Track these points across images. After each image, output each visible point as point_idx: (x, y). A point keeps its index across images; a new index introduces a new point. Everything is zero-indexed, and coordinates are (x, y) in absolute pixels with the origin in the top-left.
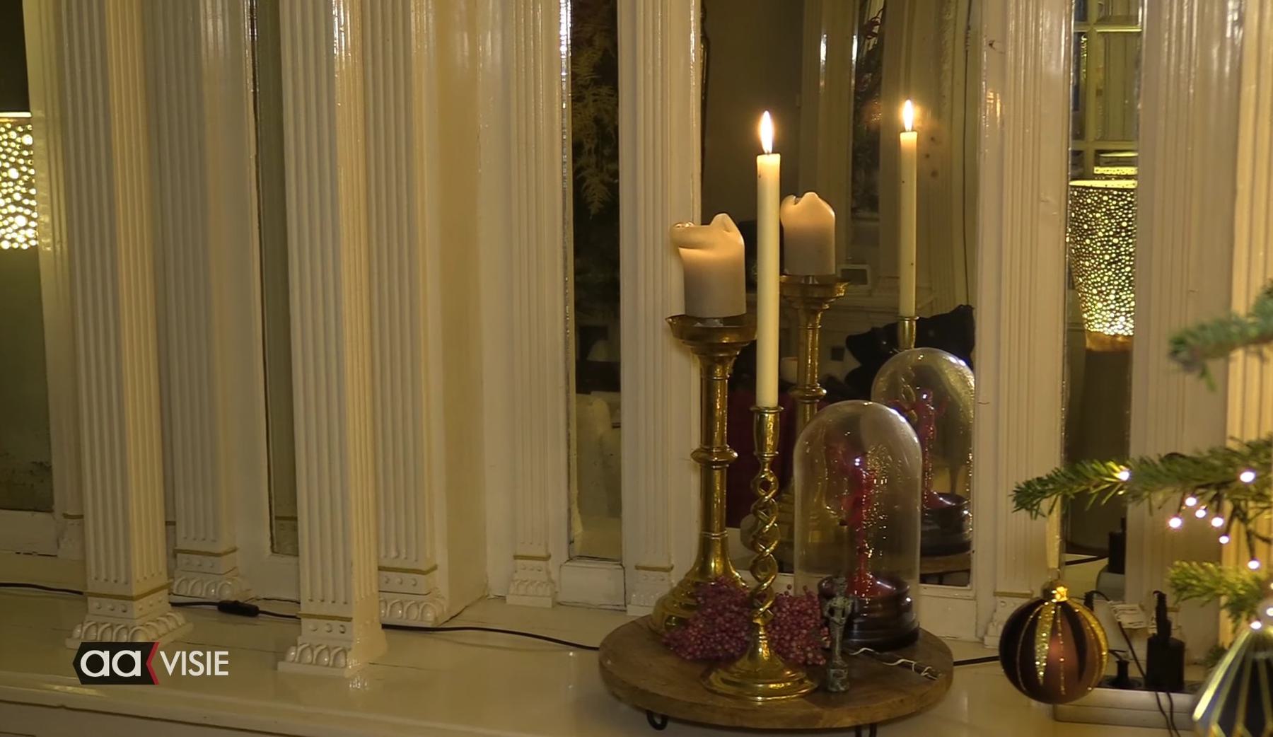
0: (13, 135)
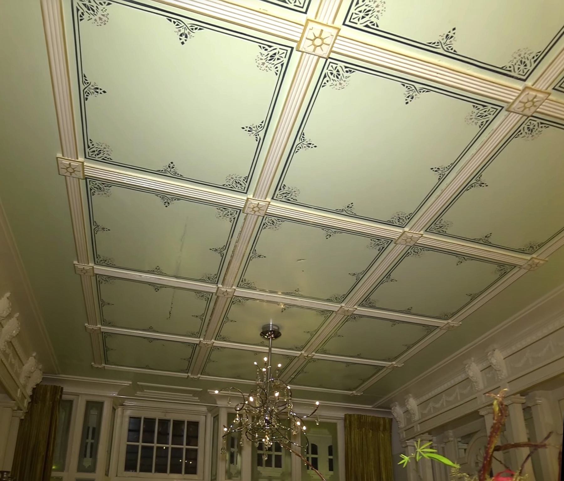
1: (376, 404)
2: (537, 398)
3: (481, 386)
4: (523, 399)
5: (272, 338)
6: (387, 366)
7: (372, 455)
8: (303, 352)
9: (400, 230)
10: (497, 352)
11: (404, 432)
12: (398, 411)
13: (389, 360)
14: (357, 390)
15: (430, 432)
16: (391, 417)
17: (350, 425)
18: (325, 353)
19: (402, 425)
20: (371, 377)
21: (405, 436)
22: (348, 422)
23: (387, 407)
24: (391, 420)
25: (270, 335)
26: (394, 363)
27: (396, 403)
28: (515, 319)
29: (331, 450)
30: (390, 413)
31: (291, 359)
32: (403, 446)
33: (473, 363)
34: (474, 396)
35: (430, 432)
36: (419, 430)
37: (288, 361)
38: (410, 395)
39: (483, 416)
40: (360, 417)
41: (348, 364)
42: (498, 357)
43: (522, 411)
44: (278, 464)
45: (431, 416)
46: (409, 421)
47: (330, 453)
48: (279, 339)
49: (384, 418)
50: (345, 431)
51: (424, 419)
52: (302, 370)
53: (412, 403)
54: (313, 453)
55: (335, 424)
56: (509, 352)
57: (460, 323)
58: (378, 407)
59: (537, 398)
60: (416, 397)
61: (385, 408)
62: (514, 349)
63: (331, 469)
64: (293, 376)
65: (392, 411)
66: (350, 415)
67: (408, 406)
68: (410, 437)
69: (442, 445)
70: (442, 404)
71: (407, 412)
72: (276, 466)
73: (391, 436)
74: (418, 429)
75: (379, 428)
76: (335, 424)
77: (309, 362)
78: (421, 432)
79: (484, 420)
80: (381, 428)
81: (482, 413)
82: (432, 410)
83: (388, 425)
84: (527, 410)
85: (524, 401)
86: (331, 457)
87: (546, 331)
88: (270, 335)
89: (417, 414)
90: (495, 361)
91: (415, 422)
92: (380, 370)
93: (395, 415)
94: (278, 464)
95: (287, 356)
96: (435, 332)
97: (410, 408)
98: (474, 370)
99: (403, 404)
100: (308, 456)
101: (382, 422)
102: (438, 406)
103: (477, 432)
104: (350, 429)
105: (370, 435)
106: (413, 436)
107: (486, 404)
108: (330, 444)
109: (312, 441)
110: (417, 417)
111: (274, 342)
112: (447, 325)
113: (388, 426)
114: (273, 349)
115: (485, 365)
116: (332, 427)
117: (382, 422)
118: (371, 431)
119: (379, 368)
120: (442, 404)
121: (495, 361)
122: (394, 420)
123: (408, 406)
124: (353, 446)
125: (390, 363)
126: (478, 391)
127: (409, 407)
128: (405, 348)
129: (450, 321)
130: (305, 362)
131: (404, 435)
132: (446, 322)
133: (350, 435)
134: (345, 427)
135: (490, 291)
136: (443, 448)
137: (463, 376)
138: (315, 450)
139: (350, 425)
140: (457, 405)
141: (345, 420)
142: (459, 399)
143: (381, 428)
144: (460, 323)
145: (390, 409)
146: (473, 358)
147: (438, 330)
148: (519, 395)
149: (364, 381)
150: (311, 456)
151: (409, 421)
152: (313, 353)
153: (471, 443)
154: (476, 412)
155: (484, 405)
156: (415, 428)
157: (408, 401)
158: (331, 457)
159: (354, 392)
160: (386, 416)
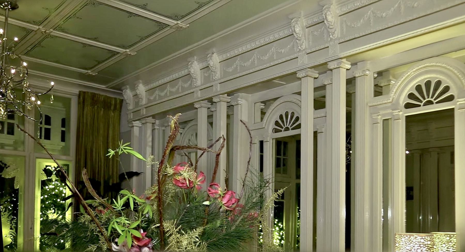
0: (444, 237)
1: (110, 84)
2: (239, 99)
3: (199, 83)
4: (228, 99)
5: (9, 9)
6: (172, 25)
7: (101, 132)
8: (41, 27)
9: (38, 27)
10: (215, 55)
11: (145, 109)
12: (128, 94)
13: (124, 47)
14: (132, 48)
15: (154, 116)
16: (122, 98)
17: (84, 102)
18: (63, 32)
19: (131, 107)
20: (107, 60)
21: (132, 117)
22: (81, 98)
23: (119, 88)
24: (122, 101)
25: (6, 6)
26: (128, 50)
27: (141, 81)
28: (181, 53)
29: (64, 123)
30: (121, 94)
31: (29, 31)
32: (130, 126)
33: (195, 62)
34: (192, 91)
35: (154, 116)
36: (219, 90)
37: (24, 33)
38: (128, 86)
39: (197, 108)
40: (94, 95)
41: (85, 45)
42: (215, 60)
43: (226, 107)
44: (11, 132)
45: (166, 99)
46: (137, 104)
47: (63, 125)
48: (16, 11)
49: (115, 99)
50: (78, 107)
51: (150, 105)
52: (39, 43)
53: (142, 89)
54: (46, 124)
55: (70, 99)
56: (345, 10)
57: (188, 25)
58: (110, 88)
59: (239, 99)
60: (146, 83)
61: (117, 90)
62: (229, 55)
63: (63, 139)
64: (29, 49)
65: (123, 93)
66: (84, 92)
67: (137, 91)
68: (137, 119)
69: (163, 128)
70: (155, 97)
71: (136, 95)
72: (8, 133)
73: (120, 115)
74: (144, 112)
75: (111, 107)
76: (70, 99)
77: (46, 37)
78: (146, 116)
79: (197, 111)
80: (112, 108)
81: (196, 106)
82: (157, 97)
83: (120, 105)
84: (230, 107)
85: (229, 100)
86: (64, 129)
87: (253, 45)
88: (6, 6)
89: (144, 99)
90: (212, 63)
91: (142, 106)
92: (114, 55)
93: (125, 97)
94: (11, 132)
95: (24, 29)
96: (117, 56)
97: (139, 93)
98: (196, 67)
99: (134, 88)
100: (41, 126)
101: (113, 102)
102: (163, 94)
103: (192, 120)
104: (84, 104)
105: (102, 112)
106: (139, 118)
107: (201, 99)
108: (64, 117)
109: (44, 113)
110: (144, 102)
111: (10, 13)
112: (177, 26)
113: (118, 106)
114: (9, 19)
115: (205, 65)
116: (66, 102)
117: (113, 102)
118: (102, 109)
119: (114, 53)
120: (155, 97)
121: (212, 63)
122: (124, 101)
123: (137, 91)
124: (85, 121)
125: (124, 50)
126: (196, 87)
127: (138, 92)
128: (139, 39)
129: (179, 22)
130: (42, 38)
131: (131, 116)
132: (176, 22)
133: (83, 110)
134: (79, 103)
135: (210, 5)
136: (164, 130)
137: (186, 72)
138: (48, 120)
139: (84, 102)
140: (178, 96)
141: (79, 96)
142: (168, 95)
143: (112, 108)
144: (188, 25)
145: (122, 91)
146: (195, 57)
147: (168, 28)
148: (151, 117)
149: (99, 63)
150: (44, 126)
151: (137, 104)
152: (51, 30)
153: (186, 129)
154: (192, 104)
155: (199, 99)
156: (214, 88)
157: (138, 86)
158: (64, 129)
159: (89, 71)
160: (118, 97)
